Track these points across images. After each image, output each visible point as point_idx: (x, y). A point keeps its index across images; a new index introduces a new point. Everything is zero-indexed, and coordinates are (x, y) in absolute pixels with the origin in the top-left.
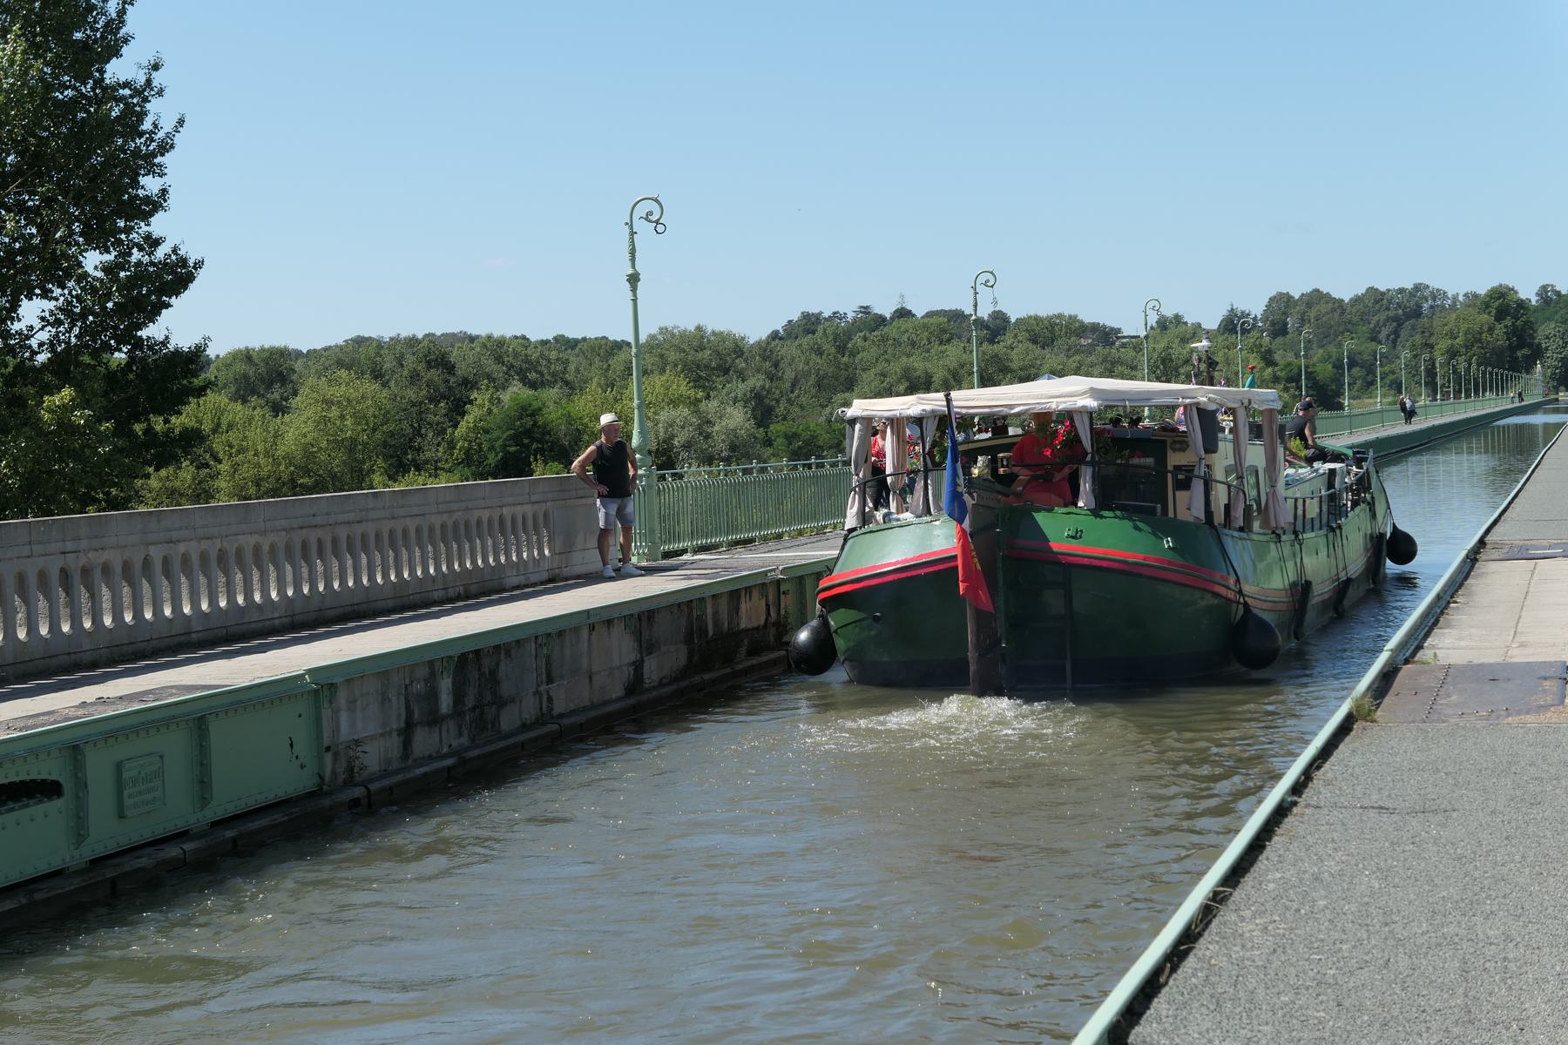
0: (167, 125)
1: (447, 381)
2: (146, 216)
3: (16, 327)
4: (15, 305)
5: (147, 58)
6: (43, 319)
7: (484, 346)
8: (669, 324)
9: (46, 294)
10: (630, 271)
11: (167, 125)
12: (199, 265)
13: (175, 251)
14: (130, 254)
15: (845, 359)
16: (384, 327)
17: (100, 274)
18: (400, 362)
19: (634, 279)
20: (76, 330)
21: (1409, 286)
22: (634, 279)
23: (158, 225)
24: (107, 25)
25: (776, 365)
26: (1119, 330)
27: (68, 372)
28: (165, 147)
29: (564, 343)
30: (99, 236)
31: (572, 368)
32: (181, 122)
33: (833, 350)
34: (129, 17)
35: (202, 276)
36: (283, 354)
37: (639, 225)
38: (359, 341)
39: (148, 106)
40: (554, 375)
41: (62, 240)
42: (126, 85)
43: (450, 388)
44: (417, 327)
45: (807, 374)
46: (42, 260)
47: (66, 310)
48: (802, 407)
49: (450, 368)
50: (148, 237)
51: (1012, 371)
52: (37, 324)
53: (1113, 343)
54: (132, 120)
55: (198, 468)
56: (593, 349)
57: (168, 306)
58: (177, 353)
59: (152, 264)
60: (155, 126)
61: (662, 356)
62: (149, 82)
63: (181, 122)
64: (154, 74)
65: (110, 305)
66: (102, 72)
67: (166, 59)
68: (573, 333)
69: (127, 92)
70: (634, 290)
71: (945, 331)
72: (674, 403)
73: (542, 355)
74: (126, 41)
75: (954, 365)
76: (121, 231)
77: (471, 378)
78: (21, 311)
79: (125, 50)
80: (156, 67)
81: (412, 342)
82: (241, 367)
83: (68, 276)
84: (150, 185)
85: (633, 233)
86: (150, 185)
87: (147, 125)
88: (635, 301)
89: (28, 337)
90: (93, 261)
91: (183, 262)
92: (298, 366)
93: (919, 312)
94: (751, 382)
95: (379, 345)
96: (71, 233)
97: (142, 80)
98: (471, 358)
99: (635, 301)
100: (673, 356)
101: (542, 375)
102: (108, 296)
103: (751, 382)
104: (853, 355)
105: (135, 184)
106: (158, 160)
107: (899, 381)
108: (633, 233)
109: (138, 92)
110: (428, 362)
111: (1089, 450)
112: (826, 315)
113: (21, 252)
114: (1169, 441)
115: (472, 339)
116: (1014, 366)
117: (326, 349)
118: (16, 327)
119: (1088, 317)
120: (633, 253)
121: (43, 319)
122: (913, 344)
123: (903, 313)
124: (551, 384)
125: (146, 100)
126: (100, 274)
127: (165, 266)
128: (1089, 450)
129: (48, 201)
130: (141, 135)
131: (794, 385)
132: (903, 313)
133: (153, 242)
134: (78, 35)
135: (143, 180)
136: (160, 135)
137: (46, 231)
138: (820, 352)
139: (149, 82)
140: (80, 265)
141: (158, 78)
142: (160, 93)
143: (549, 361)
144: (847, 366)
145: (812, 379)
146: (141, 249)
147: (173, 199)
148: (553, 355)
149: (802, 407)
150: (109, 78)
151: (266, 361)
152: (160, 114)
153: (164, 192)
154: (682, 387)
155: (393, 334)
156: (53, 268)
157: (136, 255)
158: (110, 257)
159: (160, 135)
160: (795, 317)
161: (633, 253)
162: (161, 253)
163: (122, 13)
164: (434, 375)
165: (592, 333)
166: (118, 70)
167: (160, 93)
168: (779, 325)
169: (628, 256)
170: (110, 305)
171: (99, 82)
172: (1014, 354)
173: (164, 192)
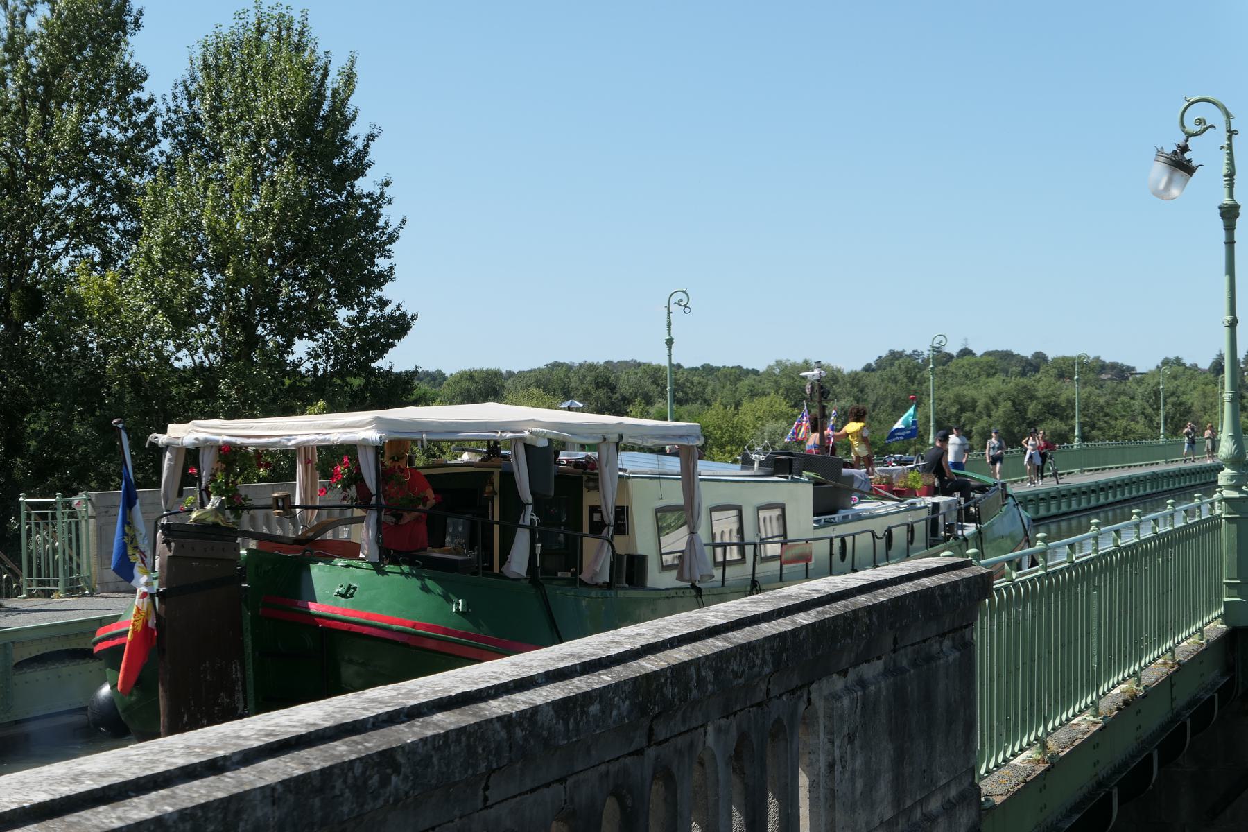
0: (394, 224)
1: (610, 398)
2: (380, 286)
3: (290, 358)
4: (290, 343)
5: (381, 178)
6: (309, 353)
7: (645, 371)
8: (783, 358)
9: (311, 338)
10: (1226, 201)
11: (394, 224)
12: (414, 317)
13: (398, 308)
14: (367, 311)
15: (915, 387)
16: (574, 357)
17: (346, 324)
18: (582, 380)
19: (670, 342)
20: (331, 362)
21: (1027, 353)
22: (670, 342)
23: (388, 291)
24: (356, 154)
25: (862, 391)
26: (1133, 369)
27: (324, 390)
28: (392, 239)
29: (708, 370)
30: (347, 298)
31: (709, 389)
32: (404, 221)
33: (905, 380)
34: (371, 149)
35: (416, 326)
36: (497, 374)
37: (674, 308)
38: (556, 365)
39: (381, 210)
40: (695, 394)
41: (322, 301)
42: (369, 195)
43: (613, 404)
44: (599, 358)
45: (884, 398)
46: (309, 314)
47: (324, 347)
48: (880, 422)
49: (613, 389)
50: (380, 300)
51: (1037, 398)
52: (305, 357)
53: (1127, 378)
54: (371, 218)
55: (428, 457)
56: (725, 376)
57: (393, 345)
58: (398, 375)
59: (383, 317)
60: (387, 224)
61: (776, 382)
62: (382, 194)
63: (404, 221)
64: (386, 189)
65: (354, 345)
66: (352, 186)
67: (394, 179)
68: (716, 362)
69: (367, 201)
70: (1230, 229)
71: (992, 367)
72: (776, 418)
73: (687, 379)
74: (369, 166)
75: (993, 393)
76: (363, 294)
77: (628, 395)
78: (294, 348)
79: (368, 172)
80: (387, 184)
81: (592, 367)
82: (465, 384)
83: (327, 325)
84: (382, 263)
85: (670, 313)
86: (382, 263)
87: (381, 223)
88: (1230, 243)
89: (298, 366)
90: (343, 314)
91: (404, 316)
92: (508, 384)
93: (979, 351)
94: (842, 403)
95: (569, 368)
96: (329, 295)
97: (377, 193)
98: (633, 378)
99: (1230, 243)
100: (785, 382)
101: (687, 394)
102: (352, 339)
103: (842, 403)
104: (920, 384)
105: (372, 263)
106: (387, 247)
107: (952, 404)
108: (670, 313)
109: (375, 201)
110: (597, 384)
111: (373, 490)
112: (908, 352)
113: (295, 308)
114: (585, 478)
115: (639, 365)
116: (1039, 394)
117: (530, 371)
118: (290, 358)
119: (1108, 358)
120: (669, 325)
121: (309, 353)
122: (967, 376)
123: (966, 352)
124: (694, 401)
125: (380, 206)
126: (346, 324)
127: (392, 318)
128: (373, 490)
129: (314, 274)
130: (376, 230)
131: (875, 405)
132: (966, 352)
133: (383, 303)
134: (336, 162)
135: (377, 261)
136: (390, 230)
137: (312, 294)
138: (895, 381)
139: (382, 194)
140: (335, 318)
141: (388, 192)
142: (390, 201)
143: (692, 383)
144: (915, 392)
145: (889, 402)
146: (375, 307)
147: (396, 270)
148: (696, 379)
149: (880, 422)
150: (357, 191)
151: (484, 379)
152: (389, 215)
153: (391, 268)
154: (783, 406)
155: (581, 361)
156: (316, 320)
157: (371, 312)
158: (354, 313)
159: (390, 230)
160: (884, 353)
161: (669, 325)
162: (388, 310)
163: (366, 146)
164: (601, 393)
165: (731, 363)
166: (363, 185)
167: (390, 201)
168: (871, 360)
169: (1223, 182)
170: (354, 345)
171: (350, 193)
172: (1039, 386)
173: (391, 268)
